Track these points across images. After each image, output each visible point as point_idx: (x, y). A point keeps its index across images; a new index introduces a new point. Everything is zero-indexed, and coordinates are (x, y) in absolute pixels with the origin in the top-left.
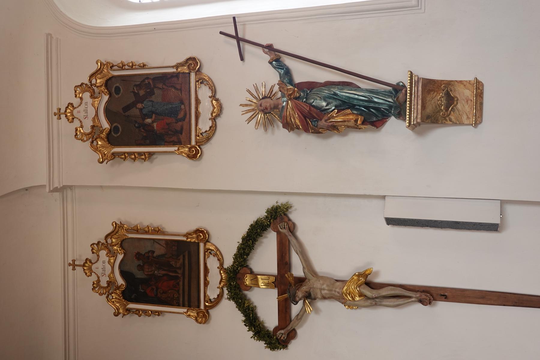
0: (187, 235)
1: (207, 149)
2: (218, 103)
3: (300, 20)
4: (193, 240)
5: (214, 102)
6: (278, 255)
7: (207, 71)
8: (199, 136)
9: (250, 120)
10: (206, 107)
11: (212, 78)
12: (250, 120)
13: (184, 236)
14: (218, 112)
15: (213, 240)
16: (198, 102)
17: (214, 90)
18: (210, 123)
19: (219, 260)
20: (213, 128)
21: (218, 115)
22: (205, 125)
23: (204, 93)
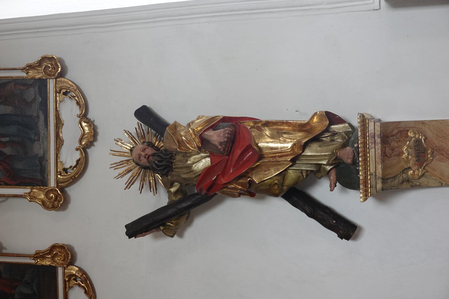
0: (39, 255)
1: (74, 191)
2: (89, 126)
3: (201, 17)
4: (48, 263)
5: (84, 124)
6: (163, 119)
7: (75, 75)
8: (60, 174)
9: (130, 184)
10: (72, 132)
11: (82, 87)
12: (130, 184)
13: (23, 69)
14: (88, 142)
15: (71, 75)
16: (59, 123)
17: (84, 106)
18: (77, 155)
19: (78, 103)
20: (82, 165)
21: (90, 144)
22: (69, 157)
23: (69, 110)
